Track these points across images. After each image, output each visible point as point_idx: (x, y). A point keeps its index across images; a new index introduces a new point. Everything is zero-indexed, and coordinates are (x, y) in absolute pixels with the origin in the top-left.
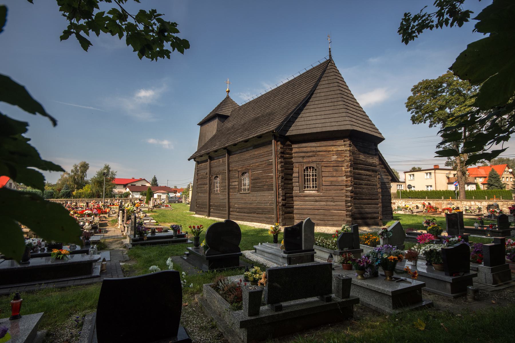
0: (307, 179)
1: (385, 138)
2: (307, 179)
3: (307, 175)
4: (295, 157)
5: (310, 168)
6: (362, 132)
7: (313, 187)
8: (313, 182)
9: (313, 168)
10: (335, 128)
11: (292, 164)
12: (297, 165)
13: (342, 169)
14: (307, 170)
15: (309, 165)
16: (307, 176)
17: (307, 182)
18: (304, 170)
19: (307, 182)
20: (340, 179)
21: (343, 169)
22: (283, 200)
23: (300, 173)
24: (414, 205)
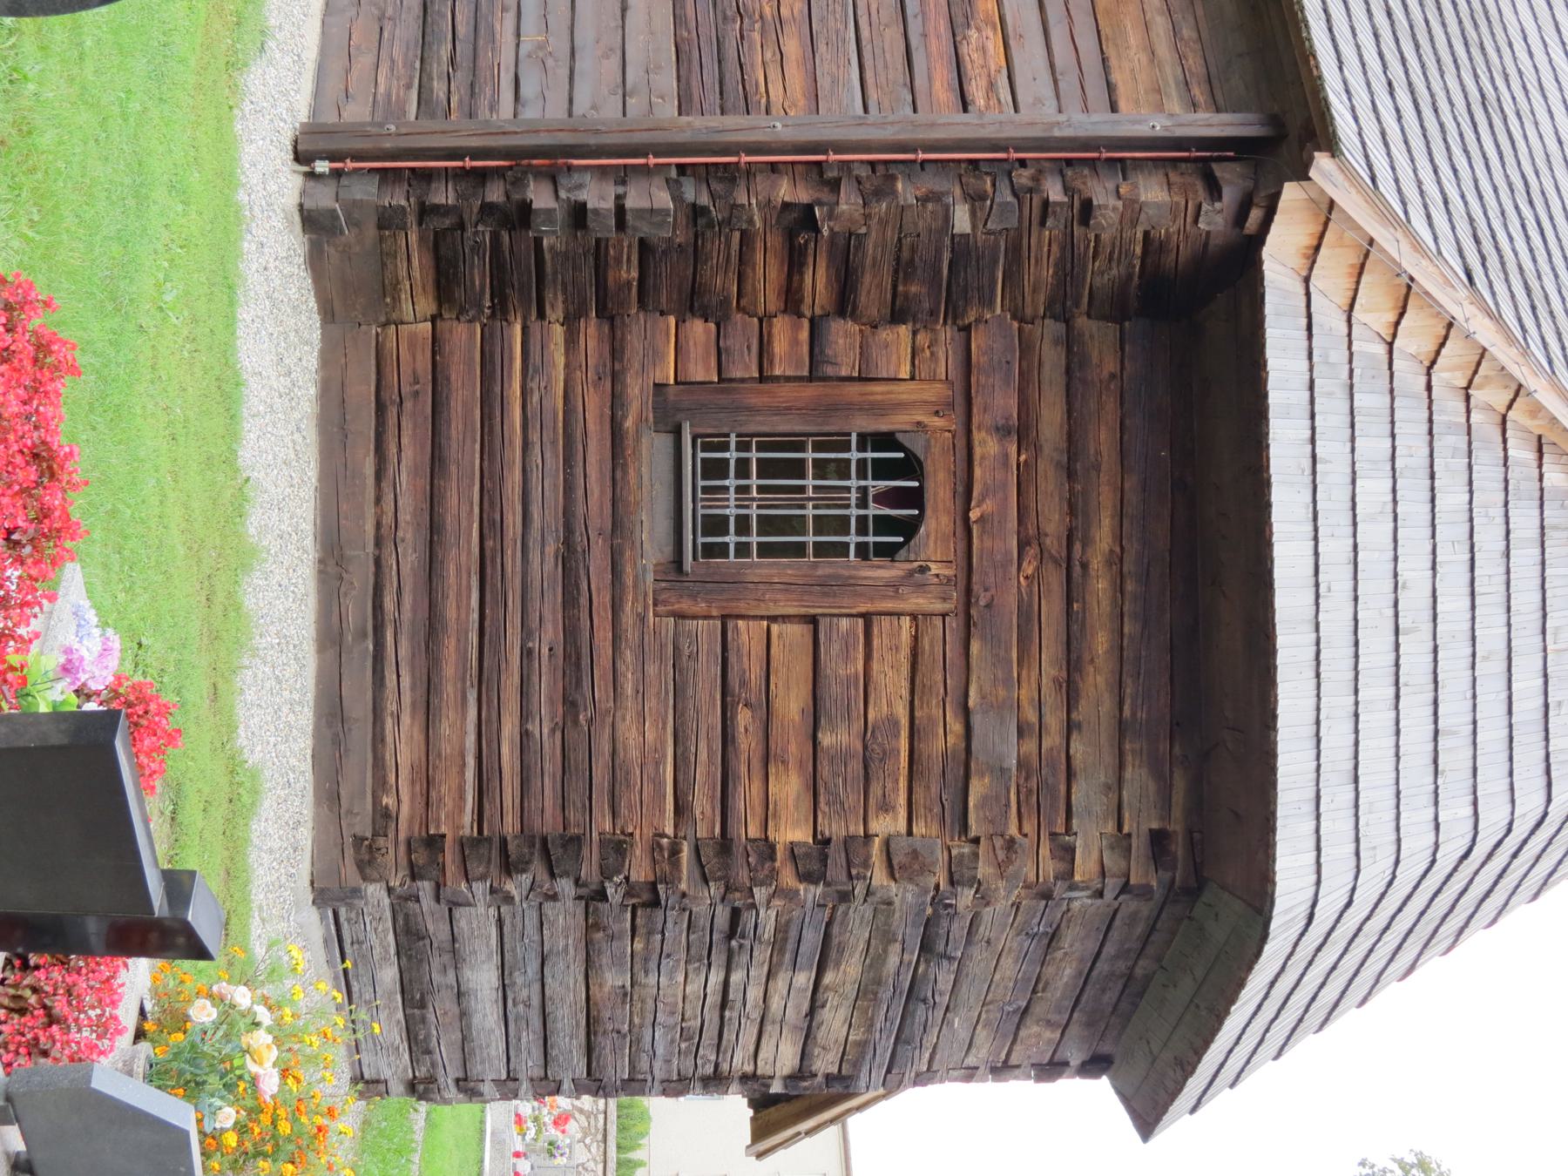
0: (797, 469)
1: (1178, 1127)
2: (797, 469)
3: (822, 524)
4: (1026, 348)
5: (915, 498)
6: (1232, 1000)
7: (716, 525)
8: (767, 524)
9: (908, 529)
10: (1277, 397)
11: (953, 313)
12: (945, 359)
13: (886, 807)
14: (883, 470)
15: (939, 488)
16: (821, 468)
17: (766, 468)
18: (885, 440)
19: (766, 468)
20: (788, 787)
21: (882, 826)
22: (579, 214)
23: (853, 390)
24: (1095, 117)
